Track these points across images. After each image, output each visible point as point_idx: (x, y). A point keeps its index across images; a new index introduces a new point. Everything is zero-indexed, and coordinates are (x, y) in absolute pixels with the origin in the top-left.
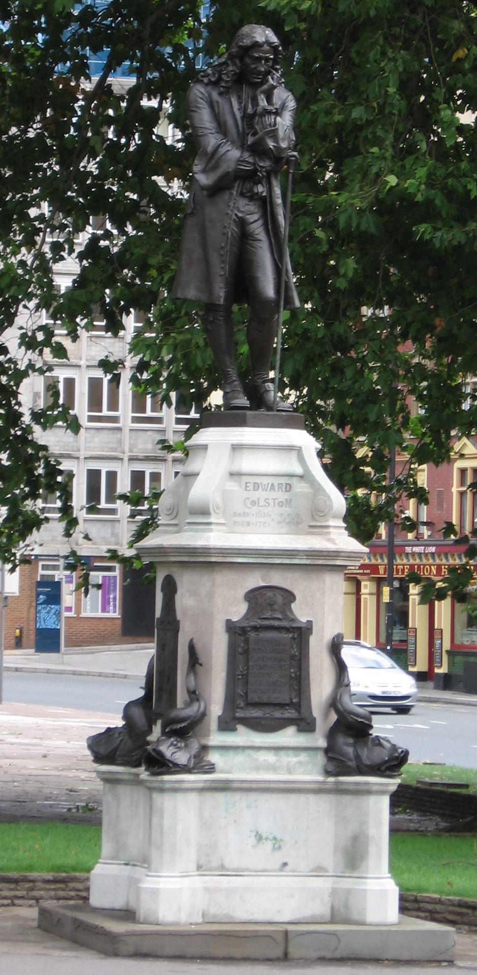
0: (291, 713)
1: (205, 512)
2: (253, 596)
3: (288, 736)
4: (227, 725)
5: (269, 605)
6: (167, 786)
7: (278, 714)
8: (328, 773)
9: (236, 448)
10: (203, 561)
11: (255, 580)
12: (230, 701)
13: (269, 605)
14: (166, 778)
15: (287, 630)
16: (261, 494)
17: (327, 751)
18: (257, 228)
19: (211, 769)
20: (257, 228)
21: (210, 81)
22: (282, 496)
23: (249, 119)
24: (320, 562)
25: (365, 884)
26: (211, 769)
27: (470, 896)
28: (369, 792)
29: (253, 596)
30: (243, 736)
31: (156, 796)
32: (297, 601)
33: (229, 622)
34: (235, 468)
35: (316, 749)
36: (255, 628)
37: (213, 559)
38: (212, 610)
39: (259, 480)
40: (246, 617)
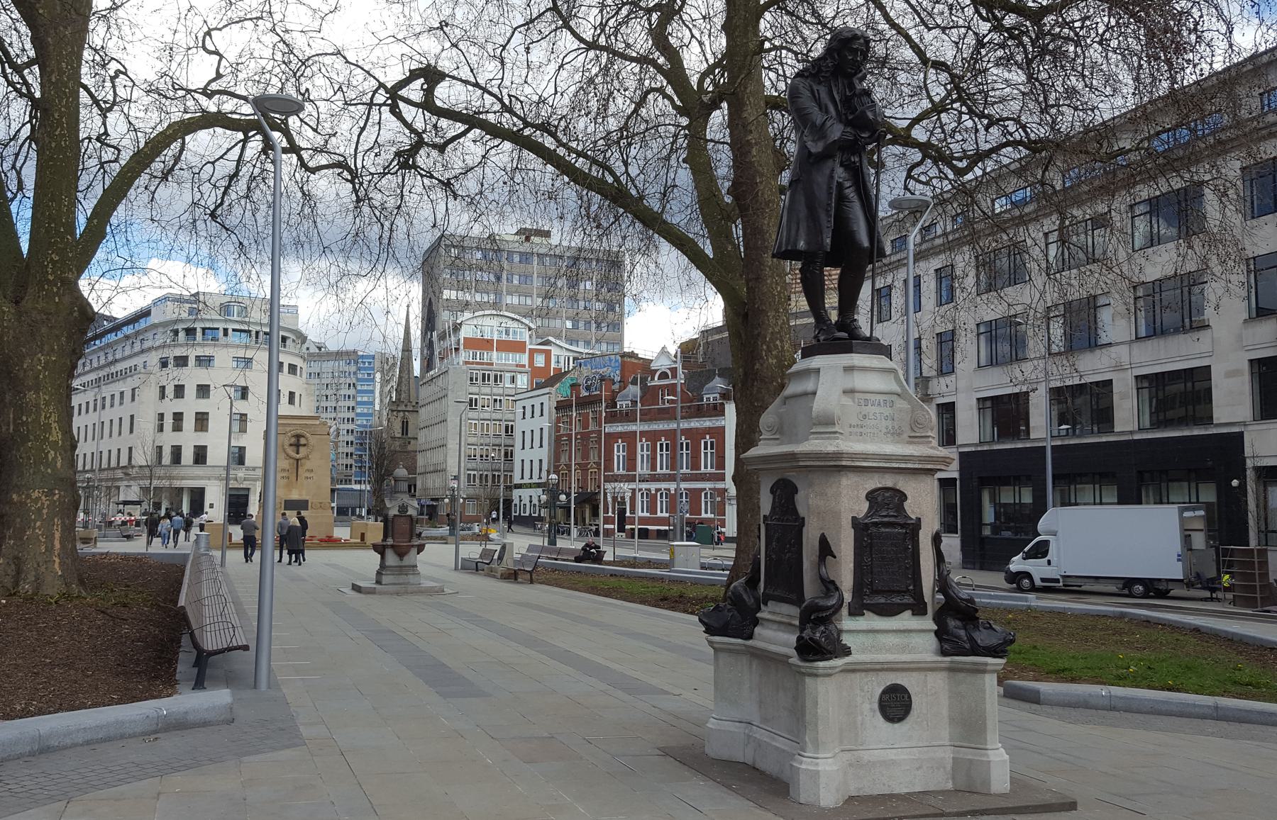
0: (908, 600)
1: (831, 422)
2: (871, 496)
3: (906, 620)
4: (855, 612)
5: (887, 501)
6: (821, 671)
7: (897, 600)
8: (944, 653)
9: (849, 369)
10: (834, 466)
11: (874, 482)
12: (858, 589)
13: (887, 501)
14: (821, 664)
15: (902, 526)
16: (871, 410)
17: (936, 633)
18: (851, 193)
19: (846, 652)
20: (851, 193)
21: (112, 489)
22: (887, 411)
23: (847, 101)
24: (903, 466)
25: (987, 755)
26: (846, 652)
27: (364, 580)
28: (984, 672)
29: (871, 496)
30: (870, 621)
31: (808, 680)
32: (909, 497)
33: (853, 518)
34: (849, 386)
35: (930, 631)
36: (876, 524)
37: (844, 463)
38: (837, 509)
39: (868, 396)
40: (866, 516)
